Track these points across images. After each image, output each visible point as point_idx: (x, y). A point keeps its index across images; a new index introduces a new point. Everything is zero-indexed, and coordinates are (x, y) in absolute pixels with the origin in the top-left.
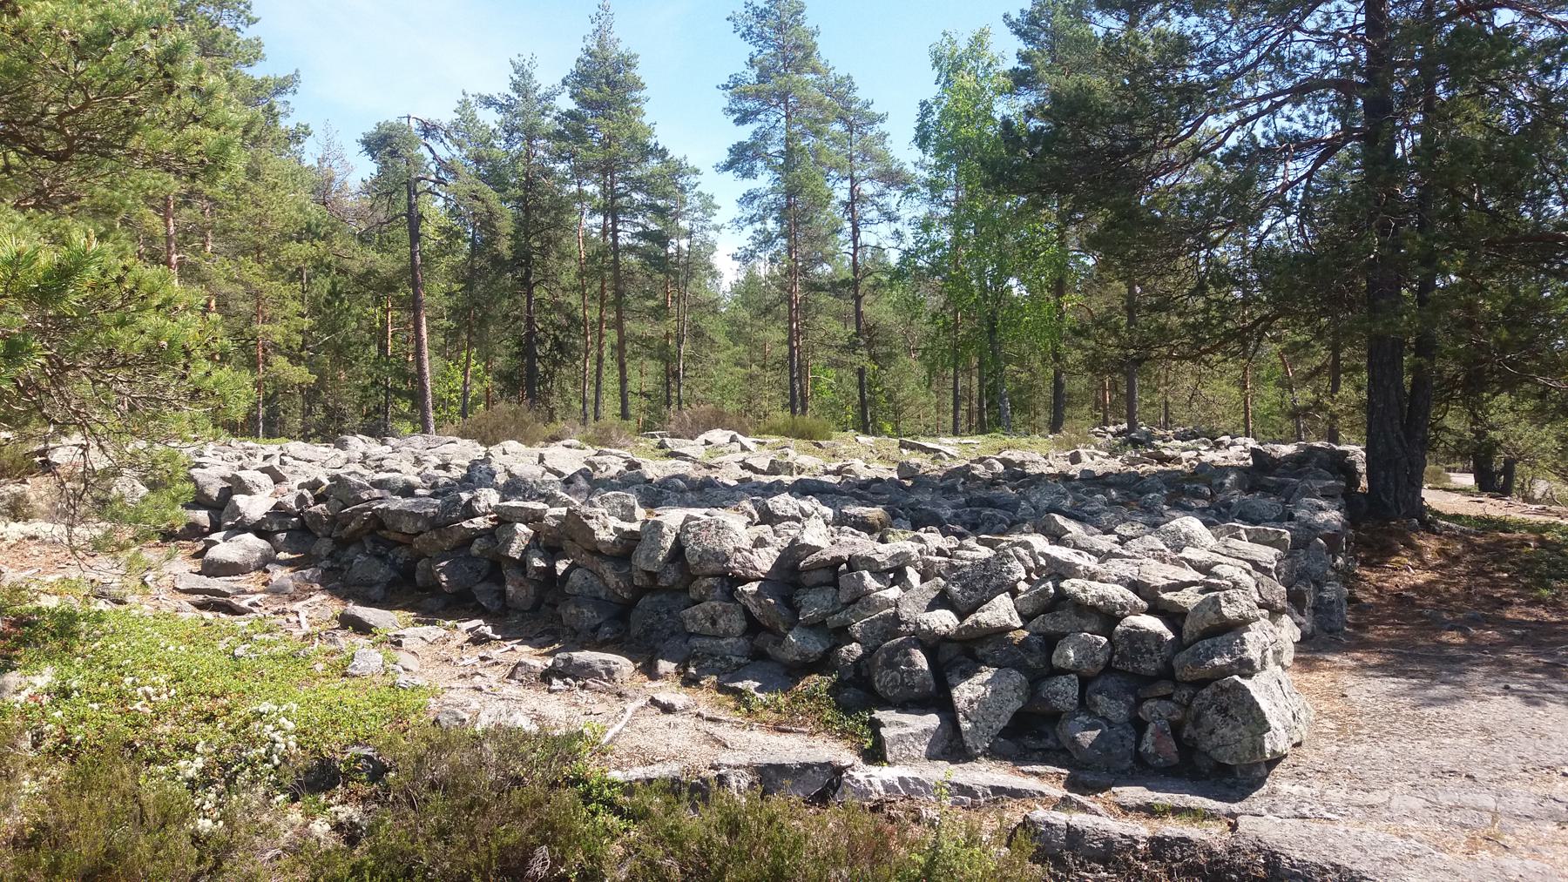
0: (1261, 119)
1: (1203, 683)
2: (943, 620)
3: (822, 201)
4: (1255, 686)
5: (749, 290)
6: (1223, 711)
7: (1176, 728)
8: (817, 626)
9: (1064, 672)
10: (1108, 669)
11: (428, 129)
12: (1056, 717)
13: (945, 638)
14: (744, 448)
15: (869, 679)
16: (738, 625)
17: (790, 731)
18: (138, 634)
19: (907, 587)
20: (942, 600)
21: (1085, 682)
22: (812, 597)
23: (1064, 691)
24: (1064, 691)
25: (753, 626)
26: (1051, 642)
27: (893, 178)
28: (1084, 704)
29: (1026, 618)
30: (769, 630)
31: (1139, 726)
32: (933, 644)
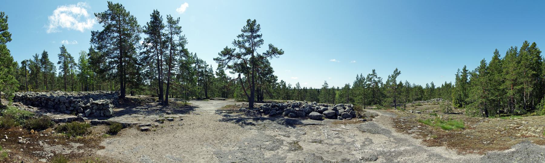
0: (169, 53)
1: (105, 109)
2: (83, 105)
3: (68, 67)
4: (110, 109)
5: (60, 77)
6: (107, 111)
7: (103, 113)
8: (73, 107)
9: (94, 109)
10: (98, 109)
11: (27, 61)
12: (93, 113)
13: (84, 107)
14: (61, 92)
15: (78, 111)
16: (65, 107)
17: (213, 100)
18: (505, 63)
19: (80, 103)
20: (84, 104)
21: (96, 110)
22: (72, 104)
23: (94, 111)
24: (94, 111)
25: (67, 107)
26: (93, 107)
27: (75, 64)
28: (96, 112)
29: (91, 105)
30: (68, 107)
31: (100, 113)
32: (83, 107)
